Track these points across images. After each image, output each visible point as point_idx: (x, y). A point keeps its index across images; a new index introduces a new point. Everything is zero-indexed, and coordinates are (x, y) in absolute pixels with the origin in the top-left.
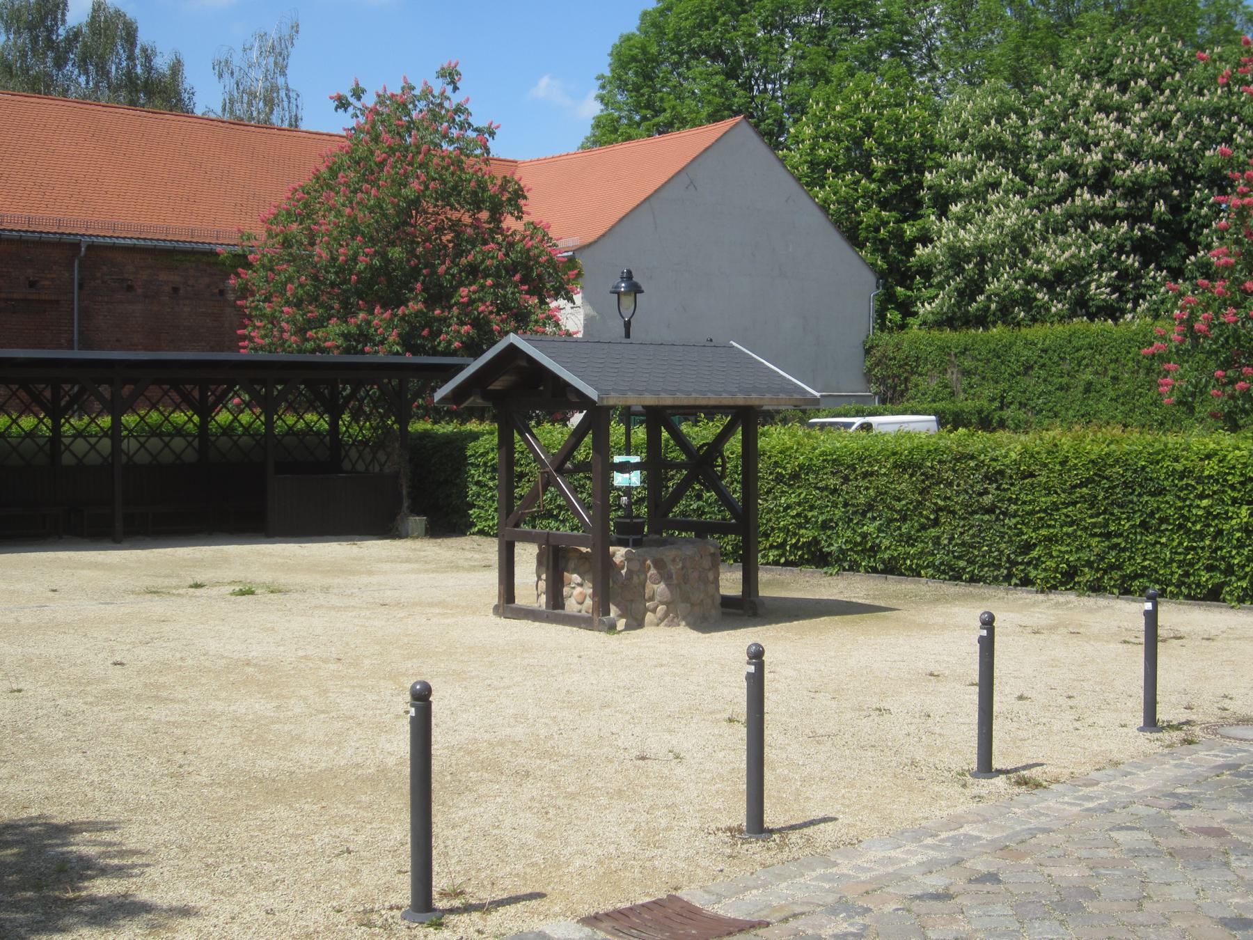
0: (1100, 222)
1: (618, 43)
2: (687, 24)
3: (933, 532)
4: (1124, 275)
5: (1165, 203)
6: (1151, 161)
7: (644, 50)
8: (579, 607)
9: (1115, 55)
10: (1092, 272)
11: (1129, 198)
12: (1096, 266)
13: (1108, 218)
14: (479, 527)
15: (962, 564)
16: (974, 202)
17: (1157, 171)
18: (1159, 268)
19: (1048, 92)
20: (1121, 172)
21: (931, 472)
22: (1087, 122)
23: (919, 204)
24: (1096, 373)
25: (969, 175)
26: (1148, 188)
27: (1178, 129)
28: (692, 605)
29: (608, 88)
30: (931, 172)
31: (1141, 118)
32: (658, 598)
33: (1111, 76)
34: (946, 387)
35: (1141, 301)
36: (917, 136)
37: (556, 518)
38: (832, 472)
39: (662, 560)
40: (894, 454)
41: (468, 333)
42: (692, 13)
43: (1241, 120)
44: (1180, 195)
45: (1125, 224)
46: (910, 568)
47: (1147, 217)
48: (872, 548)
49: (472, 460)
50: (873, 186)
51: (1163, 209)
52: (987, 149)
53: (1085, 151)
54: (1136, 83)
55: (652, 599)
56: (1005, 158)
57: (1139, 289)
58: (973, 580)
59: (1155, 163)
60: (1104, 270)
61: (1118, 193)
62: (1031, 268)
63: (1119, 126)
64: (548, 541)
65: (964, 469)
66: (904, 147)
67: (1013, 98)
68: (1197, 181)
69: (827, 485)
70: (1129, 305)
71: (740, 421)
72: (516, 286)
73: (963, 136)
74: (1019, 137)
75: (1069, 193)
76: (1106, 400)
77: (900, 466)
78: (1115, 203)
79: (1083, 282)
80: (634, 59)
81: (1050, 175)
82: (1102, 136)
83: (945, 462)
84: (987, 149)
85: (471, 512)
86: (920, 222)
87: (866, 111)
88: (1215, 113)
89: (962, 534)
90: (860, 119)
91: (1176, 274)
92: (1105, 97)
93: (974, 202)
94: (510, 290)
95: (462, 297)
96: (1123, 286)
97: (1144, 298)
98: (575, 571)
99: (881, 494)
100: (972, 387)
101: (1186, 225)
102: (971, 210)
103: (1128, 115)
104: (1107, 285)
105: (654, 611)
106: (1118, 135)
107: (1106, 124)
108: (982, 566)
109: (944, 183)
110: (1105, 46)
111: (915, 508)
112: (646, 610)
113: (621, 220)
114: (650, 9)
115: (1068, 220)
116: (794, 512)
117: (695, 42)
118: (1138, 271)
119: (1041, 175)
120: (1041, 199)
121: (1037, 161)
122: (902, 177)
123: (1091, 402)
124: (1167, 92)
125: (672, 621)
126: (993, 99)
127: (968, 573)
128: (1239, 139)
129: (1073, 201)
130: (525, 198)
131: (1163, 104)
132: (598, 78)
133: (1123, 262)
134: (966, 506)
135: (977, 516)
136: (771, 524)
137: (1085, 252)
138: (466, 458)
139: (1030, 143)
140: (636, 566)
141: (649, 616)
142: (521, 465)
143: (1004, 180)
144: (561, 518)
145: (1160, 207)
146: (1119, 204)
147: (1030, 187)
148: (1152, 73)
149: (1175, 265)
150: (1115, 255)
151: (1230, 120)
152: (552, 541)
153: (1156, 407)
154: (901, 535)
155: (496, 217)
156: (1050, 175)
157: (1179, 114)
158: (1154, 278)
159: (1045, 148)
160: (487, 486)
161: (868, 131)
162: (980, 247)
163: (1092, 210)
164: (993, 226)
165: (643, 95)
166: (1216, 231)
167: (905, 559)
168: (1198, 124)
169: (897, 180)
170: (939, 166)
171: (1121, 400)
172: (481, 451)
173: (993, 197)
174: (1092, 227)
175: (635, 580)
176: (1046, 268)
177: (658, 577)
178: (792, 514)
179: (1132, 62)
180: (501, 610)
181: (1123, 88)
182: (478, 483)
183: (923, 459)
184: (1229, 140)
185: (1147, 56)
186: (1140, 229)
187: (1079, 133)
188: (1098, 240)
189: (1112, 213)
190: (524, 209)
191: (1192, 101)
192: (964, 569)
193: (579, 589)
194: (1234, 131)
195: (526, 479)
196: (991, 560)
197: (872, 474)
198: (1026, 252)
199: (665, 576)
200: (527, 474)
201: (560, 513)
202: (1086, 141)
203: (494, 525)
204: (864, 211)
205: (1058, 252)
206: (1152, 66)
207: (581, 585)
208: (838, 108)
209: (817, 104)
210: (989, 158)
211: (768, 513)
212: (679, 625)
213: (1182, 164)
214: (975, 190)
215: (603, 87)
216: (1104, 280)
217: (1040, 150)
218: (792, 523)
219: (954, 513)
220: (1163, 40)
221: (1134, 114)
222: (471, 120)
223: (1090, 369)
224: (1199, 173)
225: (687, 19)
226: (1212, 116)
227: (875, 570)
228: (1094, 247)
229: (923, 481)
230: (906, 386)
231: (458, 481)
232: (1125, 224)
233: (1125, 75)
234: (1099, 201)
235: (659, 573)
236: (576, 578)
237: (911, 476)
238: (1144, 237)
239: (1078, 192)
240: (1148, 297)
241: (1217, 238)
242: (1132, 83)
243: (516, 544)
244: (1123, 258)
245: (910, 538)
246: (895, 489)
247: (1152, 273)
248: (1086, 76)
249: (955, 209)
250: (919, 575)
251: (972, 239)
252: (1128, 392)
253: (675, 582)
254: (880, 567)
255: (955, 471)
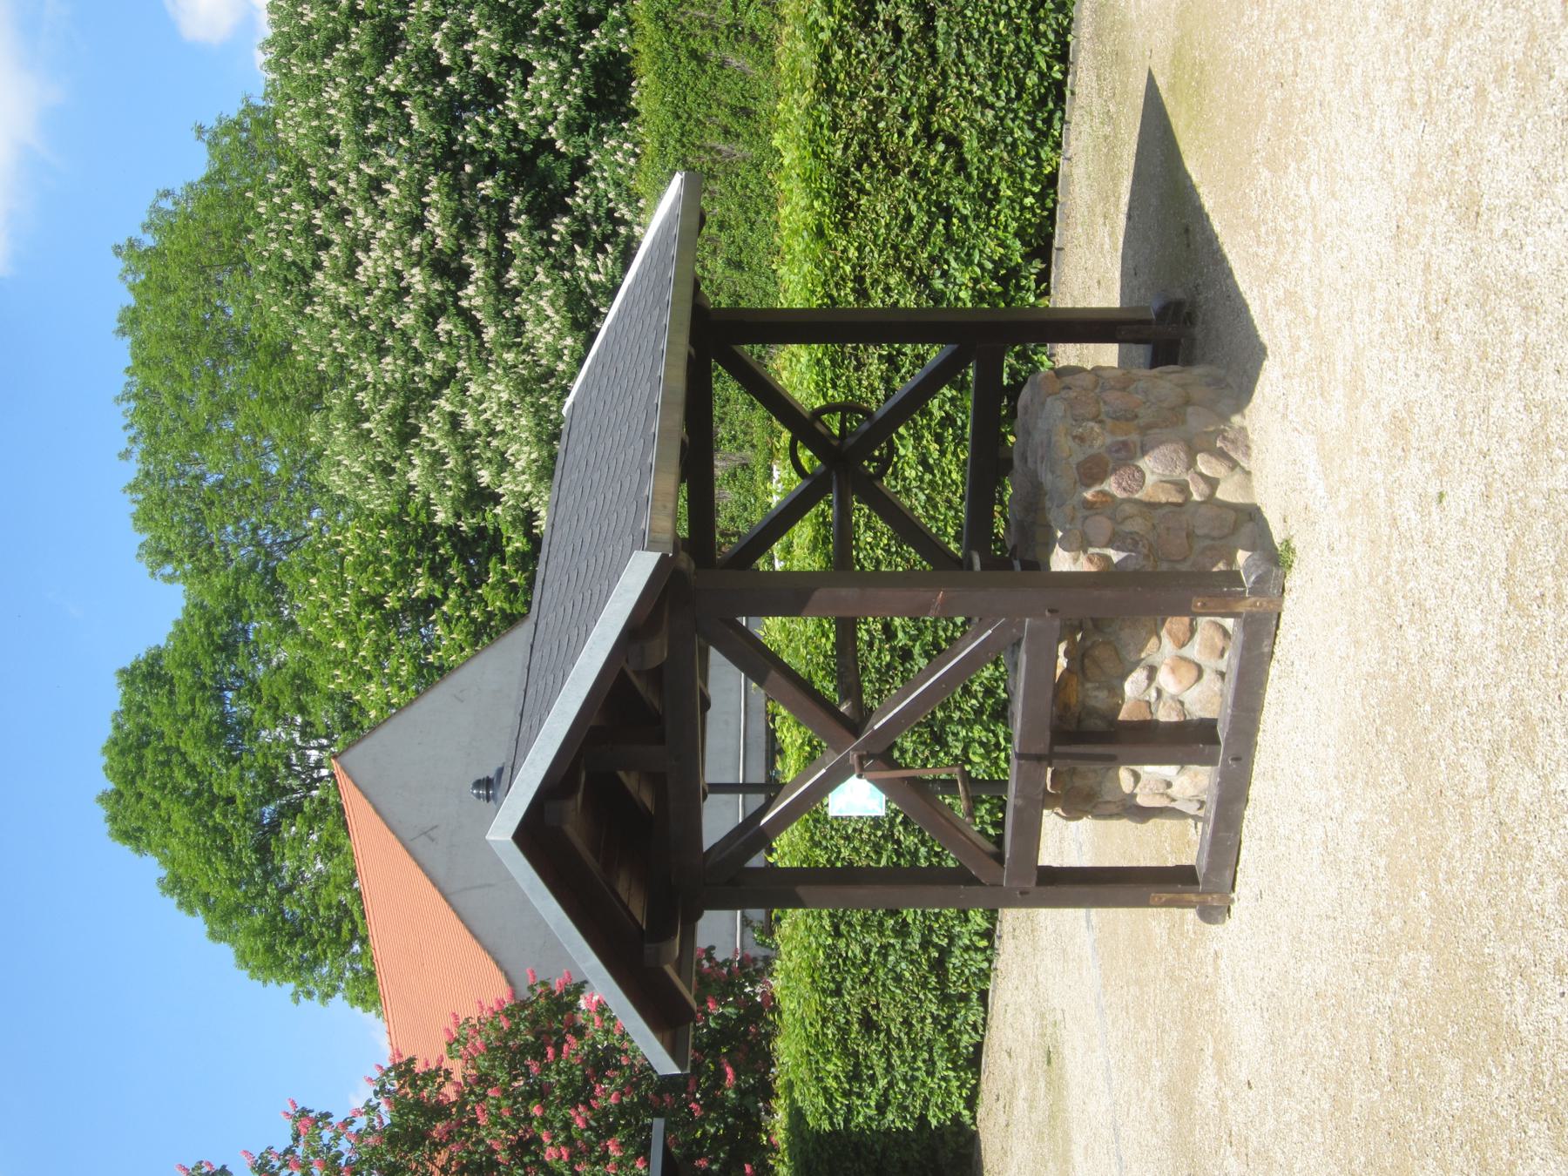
0: (507, 272)
1: (248, 971)
2: (222, 867)
3: (971, 142)
4: (580, 236)
5: (482, 180)
6: (424, 200)
7: (259, 933)
8: (1208, 676)
9: (282, 257)
10: (575, 280)
11: (475, 232)
12: (567, 275)
13: (501, 260)
14: (960, 1106)
15: (1032, 80)
16: (477, 451)
17: (438, 190)
18: (572, 191)
19: (329, 351)
20: (438, 240)
21: (855, 147)
22: (368, 292)
23: (481, 531)
24: (714, 252)
25: (439, 459)
26: (463, 205)
27: (382, 167)
28: (1188, 402)
29: (311, 986)
30: (435, 513)
31: (366, 216)
32: (1179, 473)
33: (309, 263)
34: (734, 475)
35: (616, 215)
36: (384, 534)
37: (945, 953)
38: (857, 369)
39: (1079, 466)
40: (820, 233)
41: (622, 1144)
42: (209, 861)
43: (372, 81)
44: (472, 163)
45: (510, 235)
46: (1040, 197)
47: (503, 205)
48: (1003, 281)
49: (839, 1120)
50: (452, 596)
51: (489, 183)
52: (406, 434)
53: (410, 293)
54: (319, 227)
55: (1183, 488)
56: (417, 409)
57: (600, 217)
58: (1062, 55)
59: (427, 193)
60: (574, 265)
61: (467, 246)
62: (568, 363)
63: (375, 244)
64: (1039, 758)
65: (848, 74)
66: (399, 551)
67: (336, 400)
68: (453, 141)
69: (882, 378)
70: (622, 230)
71: (736, 348)
72: (548, 1067)
73: (387, 470)
74: (389, 390)
75: (467, 316)
76: (753, 238)
77: (844, 216)
78: (480, 251)
79: (589, 291)
80: (270, 948)
81: (441, 345)
82: (387, 267)
83: (835, 116)
84: (406, 434)
85: (934, 1123)
86: (503, 528)
87: (348, 605)
88: (362, 117)
89: (973, 80)
90: (359, 615)
91: (580, 169)
92: (335, 266)
93: (477, 451)
94: (553, 1078)
95: (560, 1158)
96: (595, 239)
97: (611, 212)
98: (1117, 691)
99: (898, 259)
100: (735, 438)
101: (514, 155)
102: (489, 454)
103: (361, 235)
104: (594, 258)
105: (1213, 483)
106: (388, 248)
107: (371, 265)
108: (1037, 35)
109: (450, 494)
110: (268, 273)
111: (925, 182)
112: (1211, 499)
113: (475, 936)
114: (206, 928)
115: (504, 317)
116: (934, 447)
117: (249, 857)
118: (575, 219)
119: (441, 356)
120: (474, 356)
121: (423, 365)
122: (441, 556)
123: (756, 260)
124: (332, 183)
125: (1233, 442)
126: (337, 429)
127: (1050, 68)
128: (396, 82)
129: (476, 308)
130: (412, 1060)
131: (347, 189)
132: (297, 1001)
133: (563, 238)
134: (919, 69)
135: (940, 45)
136: (956, 500)
137: (547, 289)
138: (835, 1133)
139: (398, 375)
140: (1102, 526)
141: (1227, 493)
142: (847, 1022)
143: (449, 408)
144: (944, 943)
145: (487, 187)
146: (483, 245)
147: (459, 375)
148: (306, 206)
149: (567, 169)
150: (552, 250)
151: (372, 97)
152: (1041, 747)
153: (761, 164)
154: (977, 217)
155: (439, 1111)
156: (441, 345)
157: (361, 166)
158: (585, 198)
159: (404, 353)
160: (886, 1090)
161: (376, 602)
162: (540, 440)
163: (491, 282)
164: (510, 420)
165: (322, 935)
166: (522, 113)
167: (1023, 208)
168: (379, 140)
169: (446, 562)
170: (427, 502)
171: (752, 215)
172: (821, 1101)
173: (470, 423)
174: (514, 282)
175: (1136, 526)
176: (569, 341)
177: (1124, 472)
178: (936, 455)
179: (290, 233)
180: (1214, 900)
181: (326, 244)
182: (881, 1109)
183: (830, 166)
184: (398, 97)
185: (283, 215)
186: (517, 216)
187: (384, 304)
188: (531, 274)
189: (494, 254)
190: (433, 1066)
191: (346, 152)
192: (1042, 76)
193: (1164, 678)
194: (386, 91)
195: (873, 1012)
196: (1024, 14)
197: (859, 279)
198: (551, 373)
199: (1125, 456)
200: (864, 1010)
201: (936, 946)
202: (394, 292)
203: (958, 1078)
204: (486, 606)
205: (547, 325)
206: (296, 207)
207: (1152, 671)
208: (341, 645)
209: (335, 677)
210: (415, 431)
211: (935, 507)
212: (1243, 429)
213: (430, 160)
214: (463, 449)
215: (310, 994)
216: (586, 263)
217: (407, 360)
218: (955, 453)
219: (933, 98)
220: (263, 196)
221: (359, 226)
222: (280, 1149)
223: (708, 262)
224: (443, 138)
225: (217, 871)
226: (365, 123)
227: (1044, 276)
228: (541, 277)
229: (873, 166)
230: (733, 535)
231: (877, 1147)
232: (510, 235)
233: (307, 243)
234: (478, 273)
235: (1114, 470)
236: (1134, 685)
237: (862, 191)
238: (528, 211)
239: (465, 304)
240: (611, 205)
241: (531, 110)
242: (319, 232)
243: (1040, 864)
244: (556, 238)
245: (982, 196)
246: (887, 226)
247: (579, 200)
248: (308, 298)
249: (485, 476)
250: (1052, 180)
251: (526, 449)
252: (741, 206)
253: (1134, 437)
254: (1038, 265)
255: (853, 96)
